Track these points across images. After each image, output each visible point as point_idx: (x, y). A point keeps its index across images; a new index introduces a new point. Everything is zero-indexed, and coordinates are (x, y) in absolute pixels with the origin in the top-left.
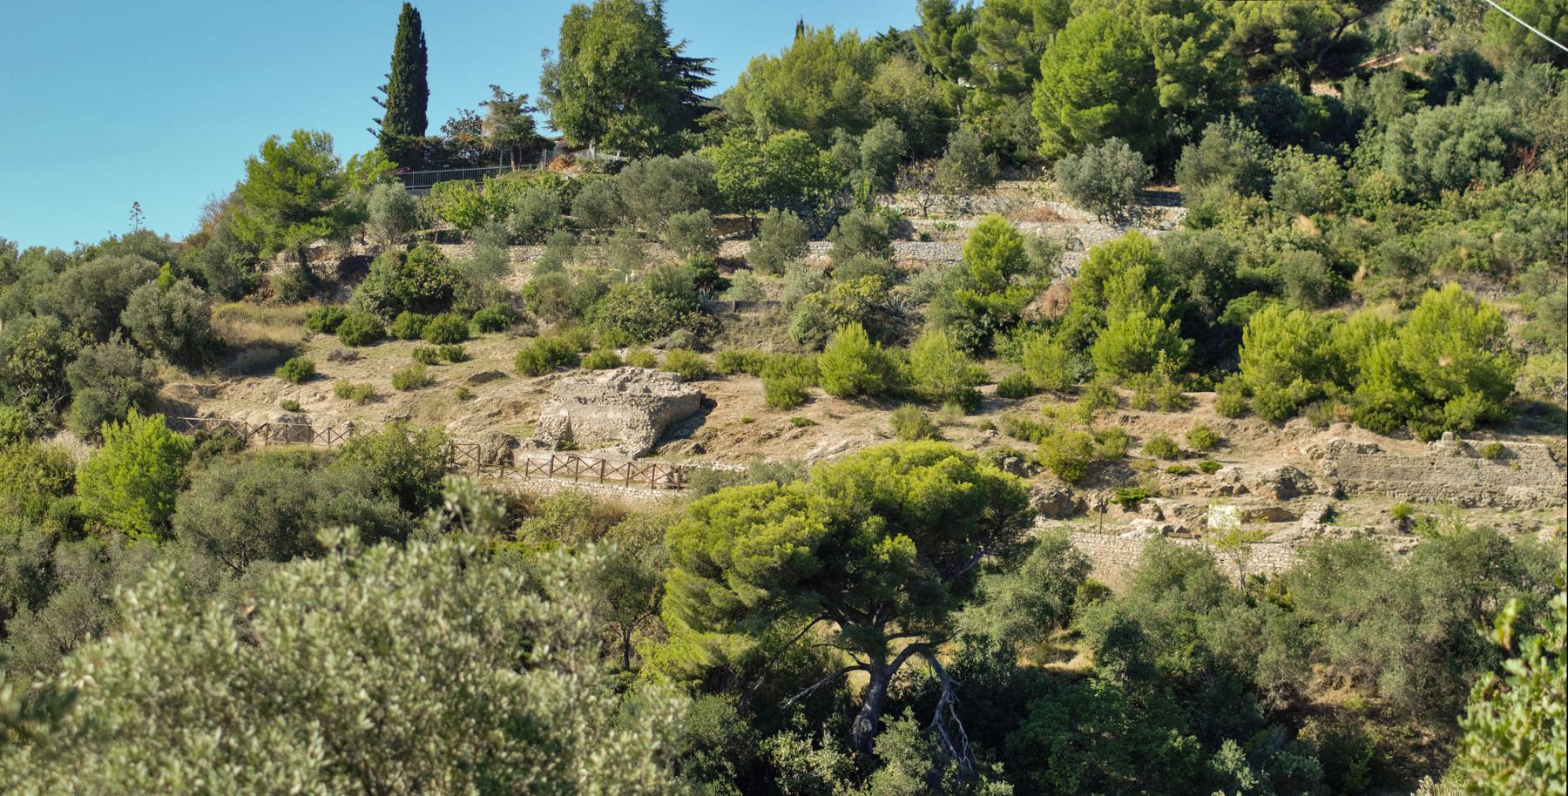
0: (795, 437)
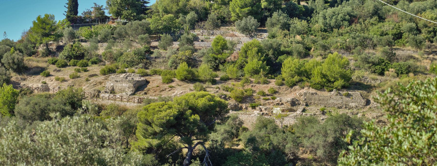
0: (170, 90)
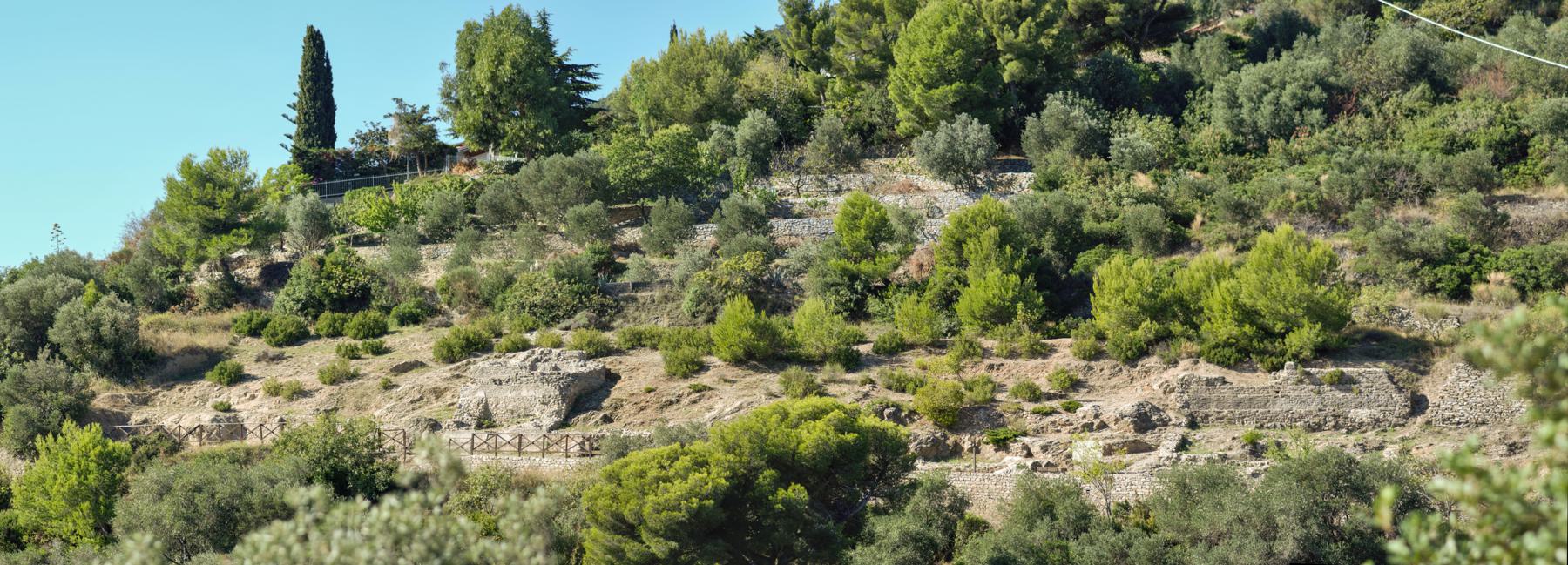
0: (694, 402)
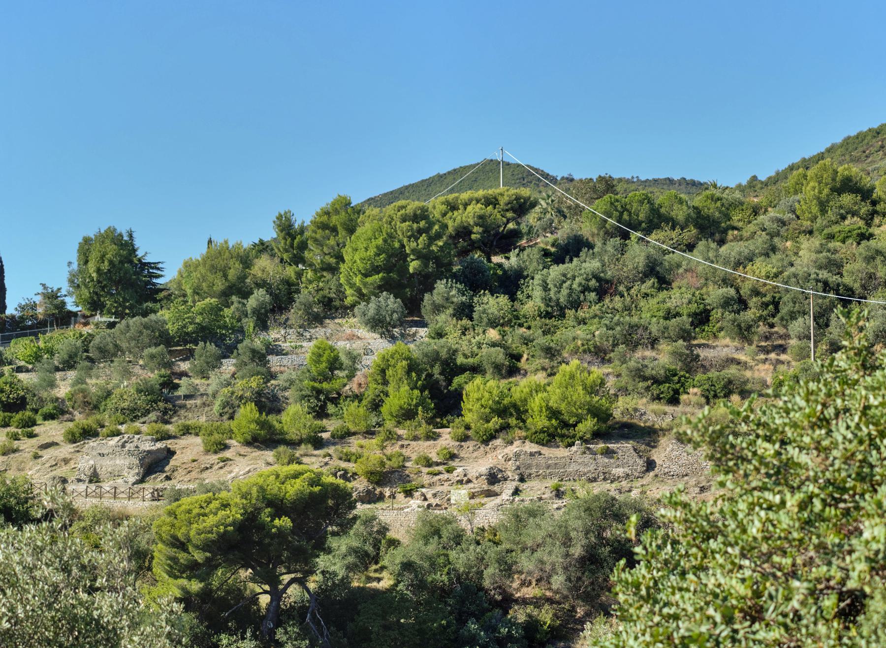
0: (221, 468)
